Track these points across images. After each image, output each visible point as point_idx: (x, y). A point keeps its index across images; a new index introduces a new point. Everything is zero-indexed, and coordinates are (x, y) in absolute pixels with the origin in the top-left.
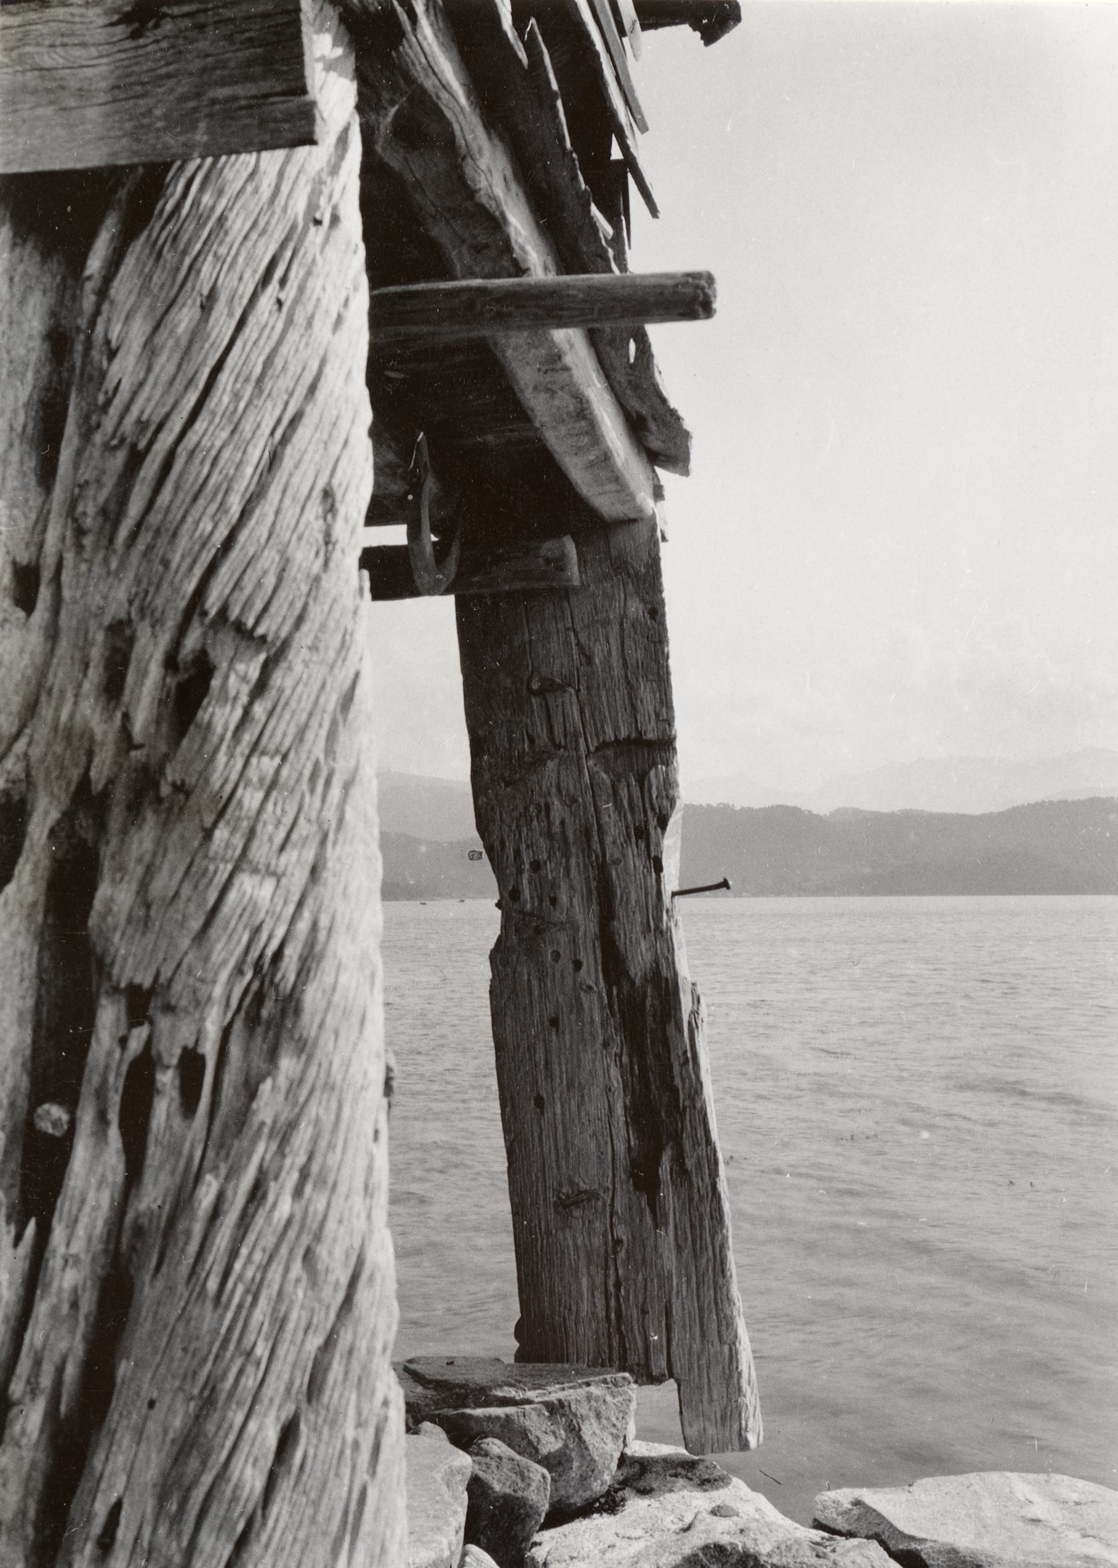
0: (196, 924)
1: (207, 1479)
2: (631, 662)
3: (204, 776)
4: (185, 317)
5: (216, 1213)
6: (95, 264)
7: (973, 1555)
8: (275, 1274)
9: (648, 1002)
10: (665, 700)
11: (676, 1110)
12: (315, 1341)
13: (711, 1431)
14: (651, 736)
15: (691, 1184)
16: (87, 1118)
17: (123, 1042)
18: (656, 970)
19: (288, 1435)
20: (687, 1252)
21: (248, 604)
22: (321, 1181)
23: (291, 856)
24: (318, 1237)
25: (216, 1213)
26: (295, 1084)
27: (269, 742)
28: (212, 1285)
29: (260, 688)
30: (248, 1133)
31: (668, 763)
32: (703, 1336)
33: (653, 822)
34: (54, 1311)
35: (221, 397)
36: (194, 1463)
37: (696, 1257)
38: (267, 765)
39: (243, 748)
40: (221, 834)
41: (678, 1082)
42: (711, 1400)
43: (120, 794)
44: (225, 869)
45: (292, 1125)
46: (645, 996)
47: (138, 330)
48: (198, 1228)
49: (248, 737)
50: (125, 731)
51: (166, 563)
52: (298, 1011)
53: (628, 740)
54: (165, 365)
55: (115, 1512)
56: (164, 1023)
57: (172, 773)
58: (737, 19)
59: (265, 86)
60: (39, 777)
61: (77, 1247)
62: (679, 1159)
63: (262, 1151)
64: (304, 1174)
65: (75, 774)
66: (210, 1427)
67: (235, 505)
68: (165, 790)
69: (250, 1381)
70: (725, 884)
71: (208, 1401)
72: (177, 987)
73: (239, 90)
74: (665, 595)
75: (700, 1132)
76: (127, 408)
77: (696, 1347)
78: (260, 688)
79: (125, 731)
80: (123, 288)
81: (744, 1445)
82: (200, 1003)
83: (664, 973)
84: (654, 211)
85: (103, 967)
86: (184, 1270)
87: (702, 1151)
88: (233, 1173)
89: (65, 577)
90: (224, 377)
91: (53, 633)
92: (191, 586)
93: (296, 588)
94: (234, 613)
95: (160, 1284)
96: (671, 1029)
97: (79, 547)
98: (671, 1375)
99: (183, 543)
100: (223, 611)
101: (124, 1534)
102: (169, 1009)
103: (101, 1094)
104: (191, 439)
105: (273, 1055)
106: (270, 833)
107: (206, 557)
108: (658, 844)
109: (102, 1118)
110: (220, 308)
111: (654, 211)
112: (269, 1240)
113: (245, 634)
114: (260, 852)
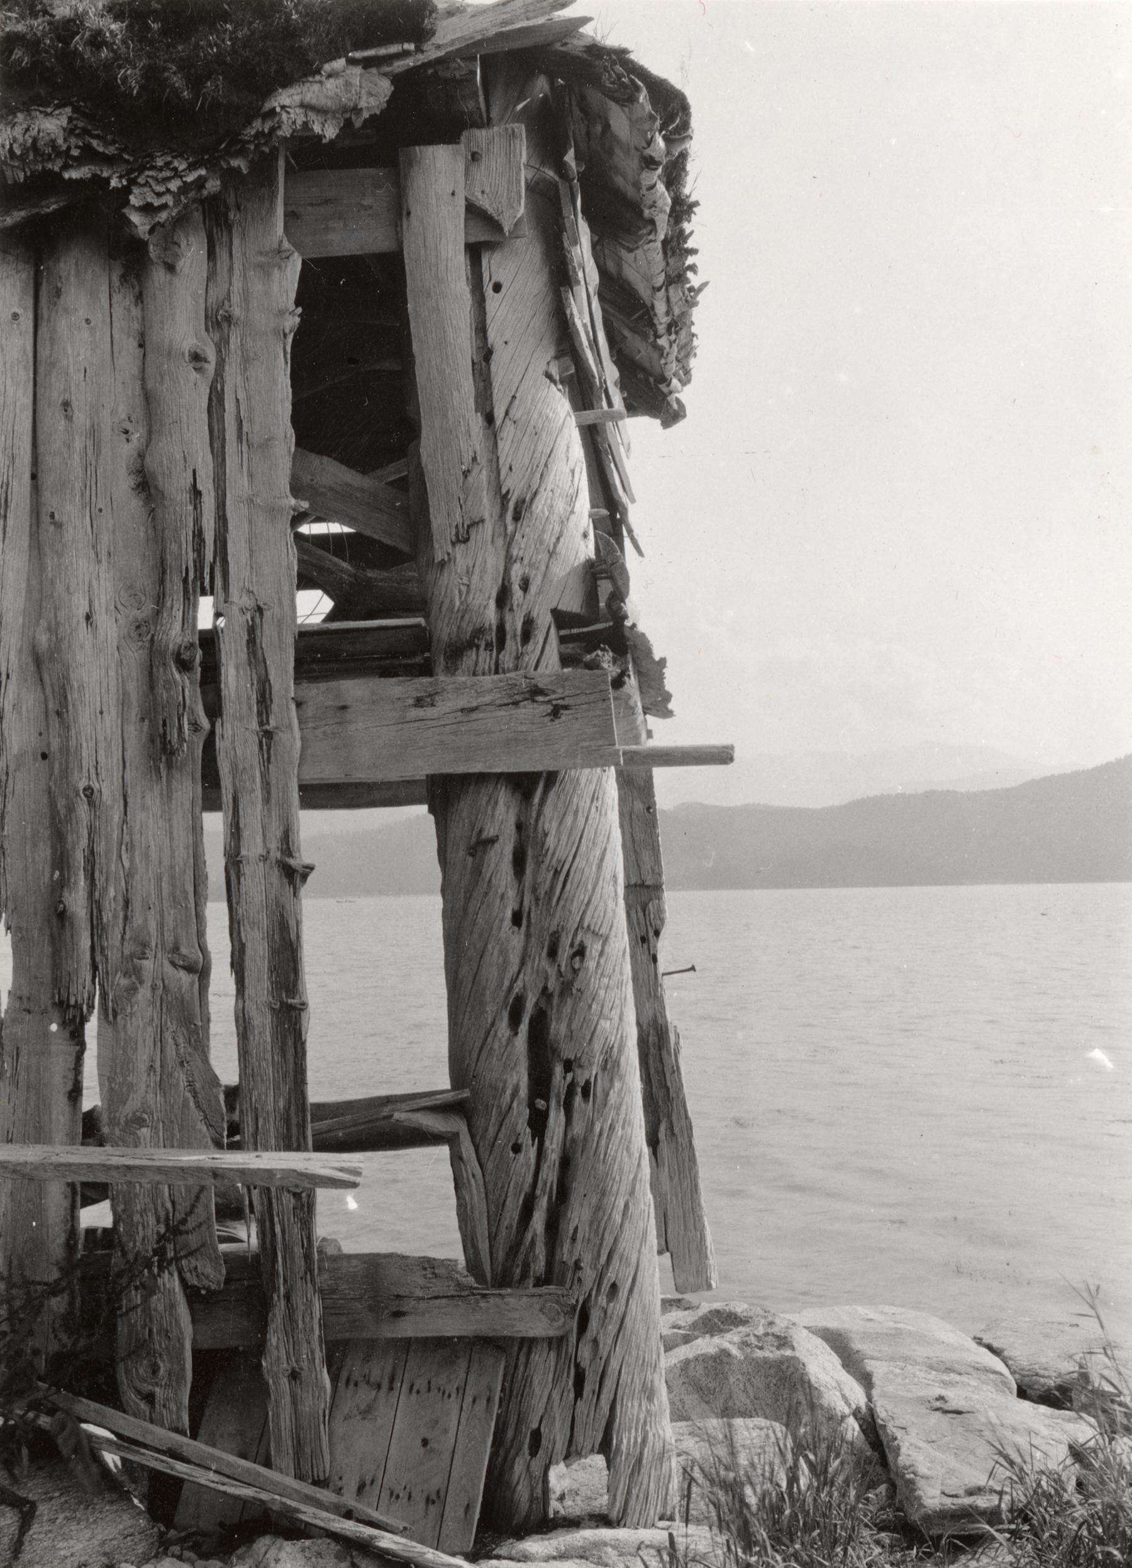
0: (588, 1038)
1: (605, 1218)
2: (637, 838)
3: (588, 985)
4: (569, 819)
5: (601, 1134)
6: (536, 800)
7: (837, 1330)
8: (619, 1154)
9: (651, 1038)
10: (658, 861)
11: (668, 1098)
12: (631, 1176)
13: (691, 1280)
14: (648, 883)
15: (677, 1143)
16: (553, 1103)
17: (565, 1078)
18: (655, 1020)
19: (626, 1206)
20: (676, 1180)
21: (596, 924)
22: (629, 1123)
23: (613, 1012)
24: (630, 1142)
25: (601, 1134)
26: (621, 1090)
27: (606, 973)
28: (602, 1157)
29: (601, 954)
30: (607, 1108)
31: (659, 898)
32: (685, 1226)
33: (651, 934)
34: (549, 1167)
35: (583, 848)
36: (601, 1213)
37: (681, 1183)
38: (606, 980)
39: (598, 976)
40: (594, 1006)
41: (669, 1084)
42: (691, 1263)
43: (556, 993)
44: (596, 1018)
45: (621, 1104)
46: (648, 1034)
47: (554, 825)
48: (596, 1139)
49: (600, 972)
50: (559, 971)
51: (570, 912)
52: (619, 1066)
53: (636, 885)
54: (564, 838)
55: (576, 1229)
56: (578, 1071)
57: (576, 985)
58: (684, 416)
59: (601, 742)
60: (528, 987)
61: (554, 1146)
62: (671, 1128)
63: (612, 1113)
64: (624, 1122)
65: (541, 986)
66: (605, 1201)
67: (590, 887)
68: (574, 991)
69: (615, 1188)
70: (693, 969)
71: (603, 1193)
72: (583, 1060)
73: (592, 743)
74: (656, 798)
75: (682, 1112)
76: (553, 854)
77: (682, 1232)
78: (601, 954)
79: (559, 971)
80: (548, 810)
81: (709, 1287)
82: (591, 1065)
83: (660, 1021)
84: (722, 756)
85: (555, 1051)
86: (592, 1152)
87: (683, 1122)
88: (605, 1120)
89: (532, 915)
90: (583, 840)
91: (528, 935)
92: (578, 919)
93: (610, 914)
94: (592, 928)
95: (584, 1156)
96: (664, 1053)
97: (537, 905)
98: (668, 1250)
99: (575, 904)
100: (589, 926)
101: (580, 1235)
102: (580, 1066)
103: (558, 1096)
104: (575, 865)
105: (611, 1081)
106: (608, 1005)
107: (583, 908)
108: (655, 947)
109: (558, 1102)
110: (580, 814)
111: (722, 756)
112: (617, 1142)
113: (595, 934)
114: (606, 1011)
